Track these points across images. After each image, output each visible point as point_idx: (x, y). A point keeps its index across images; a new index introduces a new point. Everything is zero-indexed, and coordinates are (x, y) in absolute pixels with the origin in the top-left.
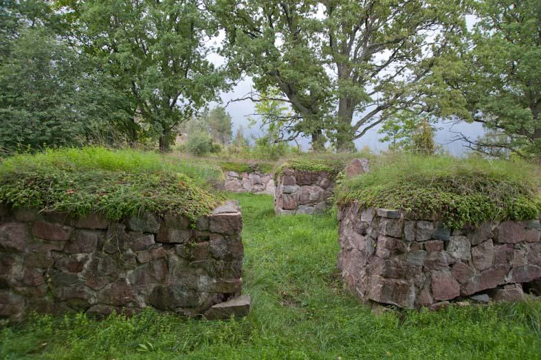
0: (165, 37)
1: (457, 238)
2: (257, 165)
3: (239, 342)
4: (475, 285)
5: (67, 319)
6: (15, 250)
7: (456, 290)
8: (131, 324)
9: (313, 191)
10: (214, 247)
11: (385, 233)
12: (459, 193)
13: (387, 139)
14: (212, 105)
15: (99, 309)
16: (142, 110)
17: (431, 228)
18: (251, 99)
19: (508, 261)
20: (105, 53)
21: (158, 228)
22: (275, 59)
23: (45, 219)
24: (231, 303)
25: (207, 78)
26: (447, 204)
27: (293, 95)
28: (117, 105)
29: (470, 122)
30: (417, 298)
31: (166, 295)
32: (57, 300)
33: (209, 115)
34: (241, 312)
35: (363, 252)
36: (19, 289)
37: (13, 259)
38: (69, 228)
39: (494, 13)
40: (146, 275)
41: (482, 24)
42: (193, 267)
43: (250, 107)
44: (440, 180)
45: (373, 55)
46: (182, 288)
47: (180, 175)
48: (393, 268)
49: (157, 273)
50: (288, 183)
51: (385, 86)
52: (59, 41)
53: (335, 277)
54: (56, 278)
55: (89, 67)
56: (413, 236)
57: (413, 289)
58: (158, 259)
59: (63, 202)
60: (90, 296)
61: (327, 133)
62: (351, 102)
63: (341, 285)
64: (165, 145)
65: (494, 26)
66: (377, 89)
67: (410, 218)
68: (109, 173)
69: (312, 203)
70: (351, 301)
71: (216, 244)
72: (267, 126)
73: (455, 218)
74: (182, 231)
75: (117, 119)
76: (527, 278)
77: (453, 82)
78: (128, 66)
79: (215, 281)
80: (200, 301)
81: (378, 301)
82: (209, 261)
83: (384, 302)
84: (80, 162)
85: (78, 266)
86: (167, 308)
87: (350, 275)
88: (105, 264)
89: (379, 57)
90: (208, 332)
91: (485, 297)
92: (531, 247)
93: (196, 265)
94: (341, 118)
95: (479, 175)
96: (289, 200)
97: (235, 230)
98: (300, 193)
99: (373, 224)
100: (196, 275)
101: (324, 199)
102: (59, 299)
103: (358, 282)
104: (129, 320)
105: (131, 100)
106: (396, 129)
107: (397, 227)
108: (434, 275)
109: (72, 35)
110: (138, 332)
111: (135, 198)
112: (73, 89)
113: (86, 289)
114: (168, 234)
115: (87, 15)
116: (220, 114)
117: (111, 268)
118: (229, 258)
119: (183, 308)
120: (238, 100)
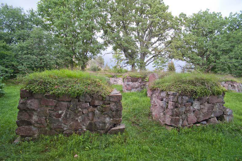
0: (84, 32)
1: (196, 102)
2: (115, 75)
3: (123, 143)
4: (202, 118)
5: (55, 137)
6: (34, 110)
7: (195, 120)
8: (81, 138)
9: (137, 84)
10: (112, 107)
11: (172, 100)
12: (196, 86)
13: (155, 66)
14: (99, 55)
15: (68, 132)
16: (75, 56)
17: (187, 98)
19: (212, 109)
20: (63, 37)
21: (91, 100)
22: (120, 40)
23: (46, 98)
24: (118, 127)
25: (97, 46)
26: (193, 90)
28: (67, 55)
29: (183, 61)
30: (182, 123)
31: (94, 126)
32: (51, 129)
34: (122, 131)
35: (162, 107)
36: (36, 125)
37: (33, 113)
38: (56, 101)
39: (189, 26)
40: (86, 118)
41: (185, 30)
42: (104, 114)
43: (111, 56)
44: (189, 81)
45: (151, 39)
46: (100, 122)
47: (98, 80)
48: (175, 113)
49: (90, 117)
50: (128, 81)
51: (155, 49)
52: (46, 33)
53: (150, 115)
54: (51, 120)
55: (57, 41)
56: (181, 101)
57: (181, 120)
58: (91, 112)
59: (53, 91)
60: (64, 127)
61: (137, 64)
62: (144, 55)
63: (152, 118)
64: (83, 68)
65: (189, 30)
66: (152, 50)
67: (180, 95)
68: (71, 79)
69: (136, 88)
70: (158, 124)
71: (112, 106)
72: (116, 62)
73: (196, 95)
74: (100, 101)
75: (67, 59)
76: (218, 115)
77: (177, 48)
78: (71, 41)
79: (112, 119)
80: (107, 127)
81: (169, 125)
82: (110, 112)
83: (171, 125)
84: (59, 75)
85: (60, 116)
86: (94, 130)
87: (156, 115)
88: (70, 115)
89: (153, 40)
90: (111, 140)
91: (205, 122)
92: (219, 104)
93: (105, 114)
95: (202, 79)
97: (120, 100)
98: (132, 85)
99: (166, 97)
100: (105, 117)
102: (52, 129)
103: (160, 117)
104: (80, 136)
105: (72, 53)
106: (158, 63)
107: (176, 98)
108: (188, 115)
109: (51, 31)
110: (84, 141)
111: (82, 89)
112: (51, 49)
113: (63, 125)
114: (94, 102)
115: (56, 24)
116: (101, 59)
117: (72, 116)
118: (117, 111)
119: (100, 130)
120: (108, 53)
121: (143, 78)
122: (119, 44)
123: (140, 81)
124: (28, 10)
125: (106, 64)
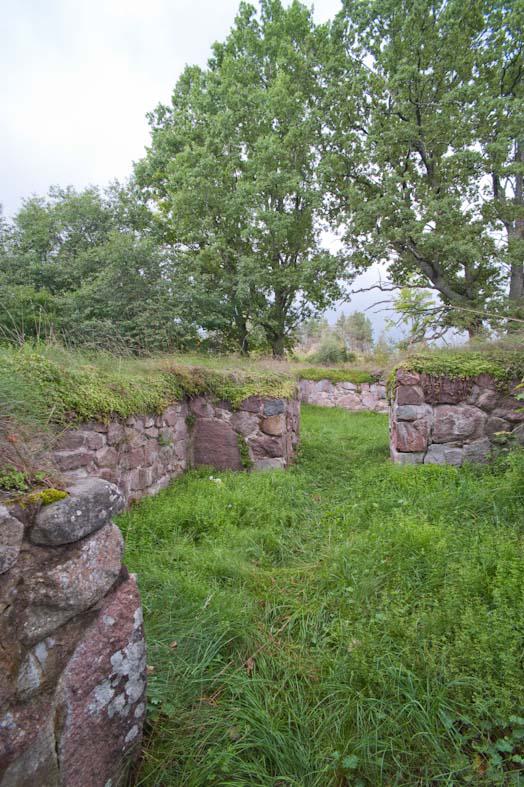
9: (461, 417)
18: (380, 288)
27: (439, 278)
33: (346, 323)
69: (460, 440)
94: (514, 302)
96: (409, 434)
98: (432, 419)
101: (487, 433)
120: (362, 290)
121: (507, 378)
122: (398, 238)
123: (482, 399)
124: (107, 185)
125: (381, 338)
